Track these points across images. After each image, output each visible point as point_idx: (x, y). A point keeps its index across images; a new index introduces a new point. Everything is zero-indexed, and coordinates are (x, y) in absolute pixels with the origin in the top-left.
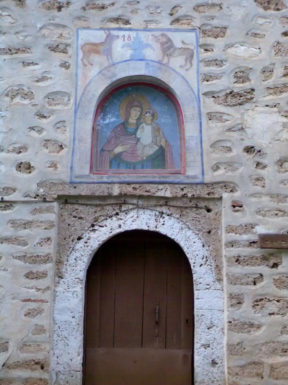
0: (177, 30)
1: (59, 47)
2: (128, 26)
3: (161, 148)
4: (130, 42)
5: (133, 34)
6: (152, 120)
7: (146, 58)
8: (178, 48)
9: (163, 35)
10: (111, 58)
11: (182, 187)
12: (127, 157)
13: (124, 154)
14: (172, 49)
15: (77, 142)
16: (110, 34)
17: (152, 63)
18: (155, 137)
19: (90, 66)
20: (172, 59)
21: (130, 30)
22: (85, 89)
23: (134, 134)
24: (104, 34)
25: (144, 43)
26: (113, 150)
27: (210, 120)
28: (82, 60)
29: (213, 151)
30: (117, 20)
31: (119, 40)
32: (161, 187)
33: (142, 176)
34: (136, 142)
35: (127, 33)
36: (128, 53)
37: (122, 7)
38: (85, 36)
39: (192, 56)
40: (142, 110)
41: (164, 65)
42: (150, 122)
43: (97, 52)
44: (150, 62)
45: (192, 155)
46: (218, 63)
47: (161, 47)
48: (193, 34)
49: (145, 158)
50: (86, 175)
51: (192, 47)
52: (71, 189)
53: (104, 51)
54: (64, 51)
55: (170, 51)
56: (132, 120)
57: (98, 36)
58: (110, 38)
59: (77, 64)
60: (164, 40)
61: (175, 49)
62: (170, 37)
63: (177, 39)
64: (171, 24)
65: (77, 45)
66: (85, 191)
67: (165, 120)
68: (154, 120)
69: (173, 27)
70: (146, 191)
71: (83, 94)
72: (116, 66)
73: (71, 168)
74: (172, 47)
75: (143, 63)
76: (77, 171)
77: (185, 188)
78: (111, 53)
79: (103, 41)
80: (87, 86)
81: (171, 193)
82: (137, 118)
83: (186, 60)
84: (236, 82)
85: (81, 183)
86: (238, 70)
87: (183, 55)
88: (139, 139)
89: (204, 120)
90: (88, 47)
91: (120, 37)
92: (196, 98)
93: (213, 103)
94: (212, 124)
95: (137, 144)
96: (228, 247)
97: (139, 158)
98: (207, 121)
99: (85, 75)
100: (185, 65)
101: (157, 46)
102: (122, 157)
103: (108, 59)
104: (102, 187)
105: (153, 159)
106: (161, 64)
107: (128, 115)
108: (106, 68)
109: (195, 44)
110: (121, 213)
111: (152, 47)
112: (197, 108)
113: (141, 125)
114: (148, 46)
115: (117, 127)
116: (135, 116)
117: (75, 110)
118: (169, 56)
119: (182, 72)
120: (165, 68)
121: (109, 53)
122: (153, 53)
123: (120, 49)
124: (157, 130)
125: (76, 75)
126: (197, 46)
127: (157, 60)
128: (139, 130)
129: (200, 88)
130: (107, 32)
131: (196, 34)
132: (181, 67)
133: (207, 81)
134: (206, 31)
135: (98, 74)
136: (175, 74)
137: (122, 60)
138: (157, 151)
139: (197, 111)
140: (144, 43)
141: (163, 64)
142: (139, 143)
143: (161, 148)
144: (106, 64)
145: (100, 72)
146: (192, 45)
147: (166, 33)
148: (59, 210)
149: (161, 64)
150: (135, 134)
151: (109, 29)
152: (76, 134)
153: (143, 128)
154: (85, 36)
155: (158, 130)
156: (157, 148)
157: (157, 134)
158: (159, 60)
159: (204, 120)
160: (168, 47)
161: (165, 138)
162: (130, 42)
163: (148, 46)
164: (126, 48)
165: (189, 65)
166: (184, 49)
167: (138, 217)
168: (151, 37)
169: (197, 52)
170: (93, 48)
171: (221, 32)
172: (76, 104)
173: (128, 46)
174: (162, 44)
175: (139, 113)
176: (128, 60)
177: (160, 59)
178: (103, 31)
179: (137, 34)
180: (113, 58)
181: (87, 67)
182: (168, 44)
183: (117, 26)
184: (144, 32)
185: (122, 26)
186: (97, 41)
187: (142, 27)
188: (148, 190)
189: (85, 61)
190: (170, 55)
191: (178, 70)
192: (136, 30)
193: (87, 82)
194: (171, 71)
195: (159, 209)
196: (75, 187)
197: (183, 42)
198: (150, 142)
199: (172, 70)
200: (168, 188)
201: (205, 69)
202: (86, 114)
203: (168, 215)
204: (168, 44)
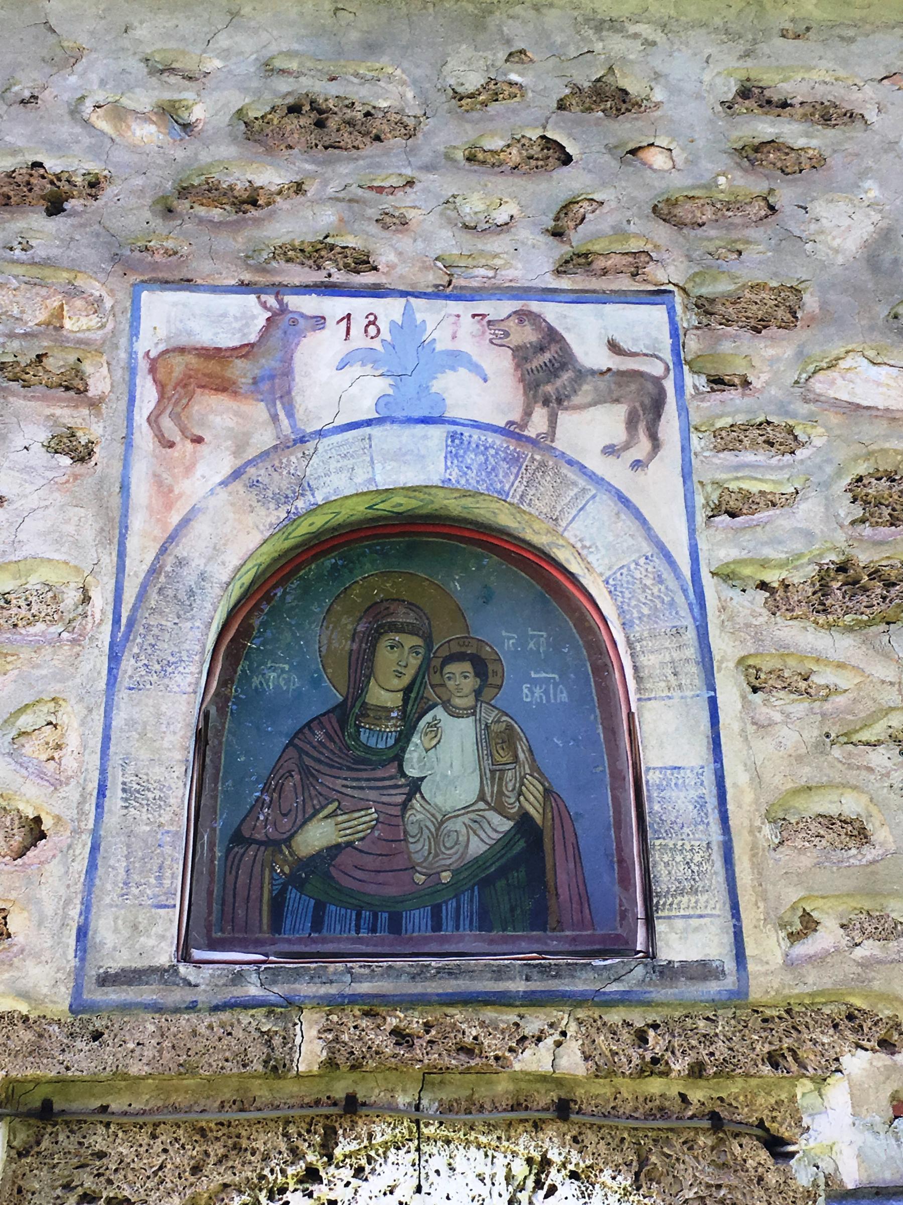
0: (580, 297)
1: (48, 362)
2: (368, 278)
3: (524, 822)
4: (376, 344)
5: (389, 310)
6: (478, 693)
7: (449, 414)
8: (593, 372)
9: (522, 316)
10: (290, 415)
11: (639, 1024)
12: (359, 874)
13: (343, 858)
14: (566, 376)
15: (115, 800)
16: (284, 309)
17: (476, 435)
18: (493, 772)
19: (189, 446)
20: (565, 418)
21: (376, 292)
22: (163, 550)
23: (392, 760)
24: (258, 310)
25: (439, 347)
26: (288, 841)
27: (755, 690)
28: (153, 420)
29: (781, 843)
30: (316, 253)
31: (325, 333)
32: (534, 1023)
33: (439, 970)
34: (400, 799)
35: (360, 306)
36: (366, 392)
37: (337, 199)
38: (170, 317)
39: (657, 406)
40: (429, 645)
41: (533, 442)
42: (470, 701)
43: (224, 387)
44: (467, 431)
45: (679, 858)
46: (779, 439)
47: (518, 366)
48: (657, 314)
49: (446, 877)
50: (153, 970)
51: (656, 369)
52: (79, 1044)
53: (255, 381)
54: (73, 385)
55: (559, 383)
56: (384, 694)
57: (224, 318)
58: (282, 327)
59: (128, 441)
60: (528, 335)
61: (582, 374)
62: (553, 324)
63: (588, 333)
64: (558, 272)
65: (132, 354)
66: (149, 1053)
67: (538, 692)
68: (488, 692)
69: (564, 283)
70: (462, 1049)
71: (154, 571)
72: (311, 445)
73: (82, 933)
74: (563, 366)
75: (437, 433)
76: (115, 949)
77: (655, 1026)
78: (289, 392)
79: (253, 338)
80: (173, 538)
81: (586, 1059)
82: (406, 680)
83: (631, 423)
84: (863, 521)
85: (125, 1008)
86: (862, 469)
87: (617, 401)
88: (415, 786)
89: (730, 691)
90: (179, 365)
91: (331, 323)
92: (685, 591)
93: (765, 612)
94: (775, 706)
95: (405, 806)
96: (620, 386)
97: (420, 878)
98: (744, 697)
99: (165, 492)
100: (627, 446)
101: (498, 364)
102: (334, 872)
103: (275, 418)
104: (238, 1033)
105: (486, 883)
106: (519, 438)
107: (361, 667)
108: (265, 455)
109: (668, 356)
110: (332, 1169)
111: (476, 368)
112: (691, 635)
113: (428, 718)
114: (456, 359)
115: (308, 725)
116: (399, 675)
117: (112, 645)
118: (557, 403)
119: (614, 472)
120: (538, 457)
121: (277, 387)
122: (484, 391)
123: (332, 374)
124: (499, 743)
125: (125, 488)
126: (678, 364)
127: (502, 424)
128: (416, 739)
129: (703, 545)
130: (271, 301)
131: (671, 312)
132: (610, 450)
133: (733, 515)
134: (712, 301)
135: (224, 483)
136: (582, 482)
137: (341, 421)
138: (507, 840)
139: (692, 652)
140: (439, 347)
141: (528, 439)
142: (416, 803)
143: (524, 822)
144: (265, 439)
145: (236, 474)
146: (657, 357)
147: (535, 306)
148: (10, 1160)
149: (519, 438)
150: (399, 759)
151: (279, 290)
152: (115, 759)
153: (434, 726)
154: (170, 317)
155: (508, 739)
156: (506, 825)
157: (504, 757)
158: (511, 423)
159: (730, 691)
160: (547, 370)
161: (542, 778)
162: (376, 344)
163: (456, 359)
164: (355, 370)
165: (644, 444)
166: (621, 374)
167: (419, 1189)
168: (468, 325)
169: (680, 389)
170: (205, 371)
171: (777, 312)
172: (116, 621)
173: (367, 357)
174: (521, 355)
175: (415, 662)
176: (369, 423)
177: (516, 416)
178: (253, 298)
179: (408, 312)
180: (300, 414)
181: (175, 453)
182: (547, 356)
183: (319, 277)
184: (440, 303)
185: (339, 277)
186: (227, 341)
187: (430, 279)
188: (469, 1040)
189: (167, 423)
190: (559, 401)
191: (596, 463)
192: (404, 294)
193: (175, 519)
194: (565, 470)
195: (525, 1145)
196: (97, 1036)
197: (614, 347)
198: (473, 797)
199: (571, 462)
200: (572, 1029)
201: (716, 467)
202: (166, 668)
203: (574, 1175)
204: (547, 356)
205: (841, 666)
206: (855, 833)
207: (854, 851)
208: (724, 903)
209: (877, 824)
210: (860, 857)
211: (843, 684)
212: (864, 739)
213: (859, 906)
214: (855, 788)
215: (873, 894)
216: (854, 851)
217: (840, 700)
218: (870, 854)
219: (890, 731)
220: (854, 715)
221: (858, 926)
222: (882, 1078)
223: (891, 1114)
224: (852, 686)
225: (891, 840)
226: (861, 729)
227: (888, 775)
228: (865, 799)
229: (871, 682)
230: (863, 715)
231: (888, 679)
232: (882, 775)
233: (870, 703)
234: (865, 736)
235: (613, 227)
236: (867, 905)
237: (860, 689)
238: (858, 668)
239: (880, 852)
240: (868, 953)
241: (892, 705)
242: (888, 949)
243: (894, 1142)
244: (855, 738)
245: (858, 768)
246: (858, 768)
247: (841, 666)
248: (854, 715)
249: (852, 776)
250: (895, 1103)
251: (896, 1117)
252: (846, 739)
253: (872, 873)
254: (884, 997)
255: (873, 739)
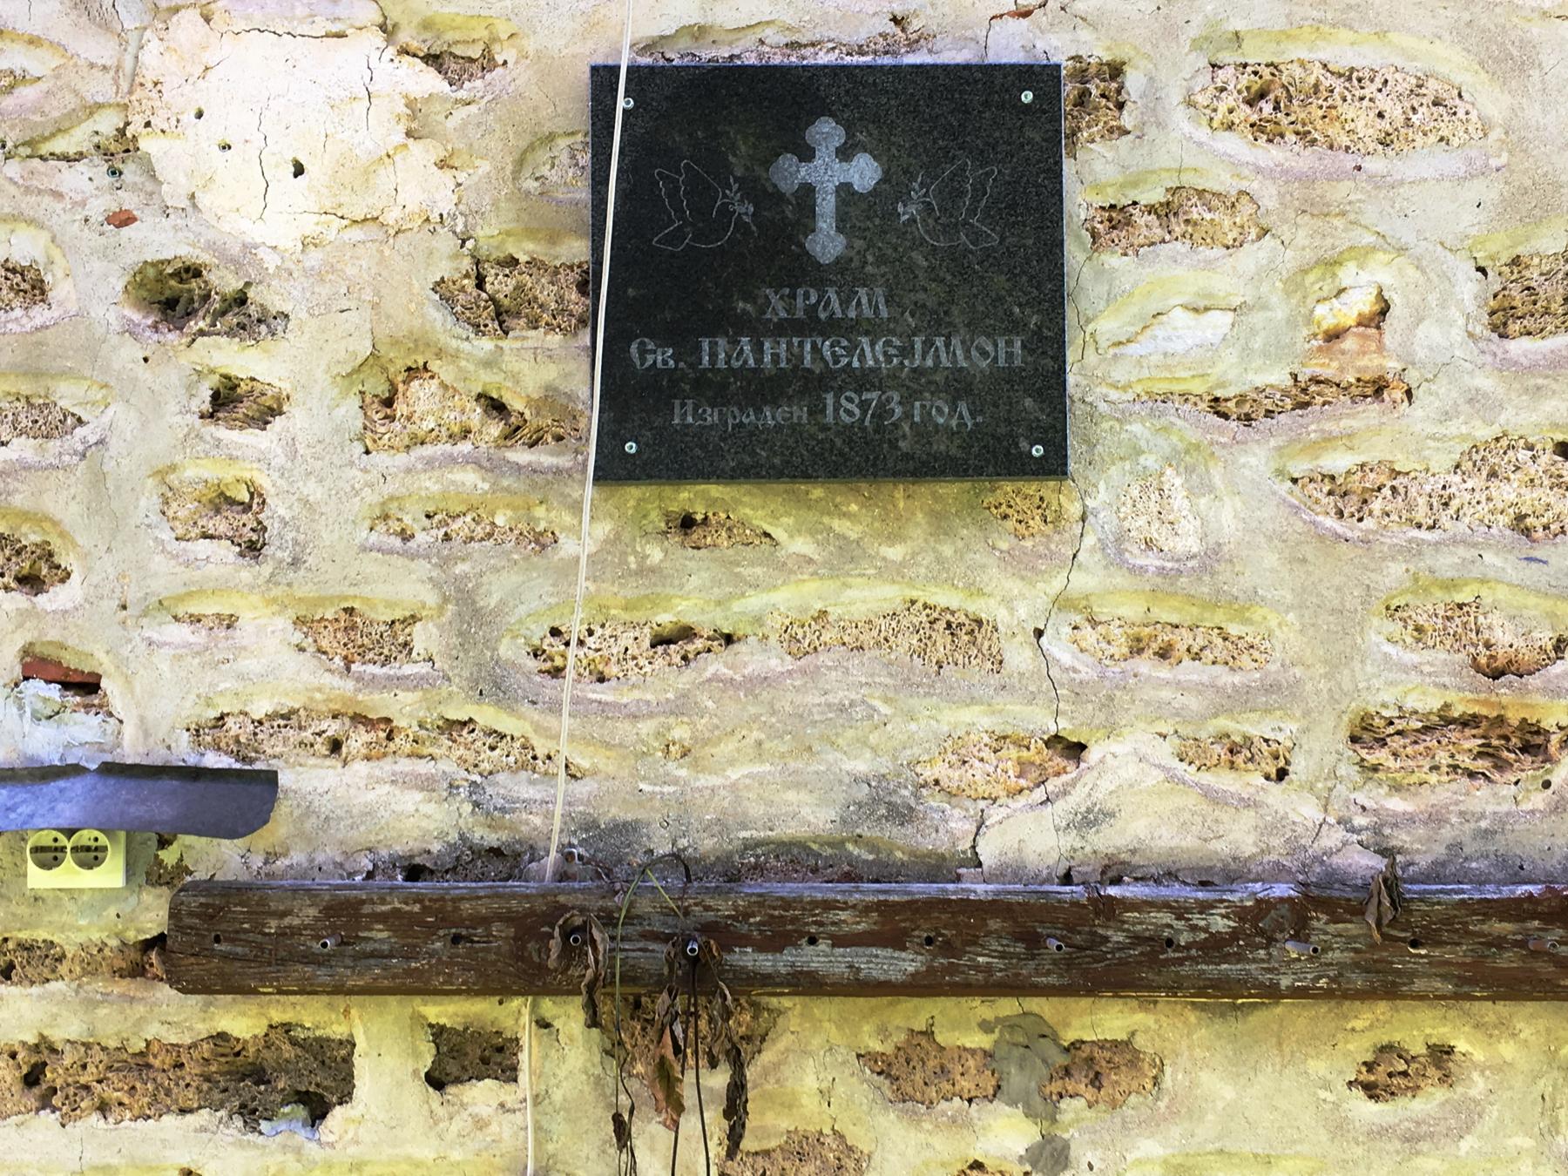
205: (34, 41)
206: (24, 286)
207: (18, 312)
208: (750, 493)
209: (60, 274)
210: (25, 320)
211: (35, 70)
212: (58, 151)
213: (14, 390)
214: (31, 222)
215: (37, 374)
216: (18, 312)
217: (27, 93)
218: (40, 315)
219: (96, 139)
220: (43, 113)
221: (10, 417)
222: (11, 627)
223: (18, 672)
224: (48, 72)
225: (73, 297)
226: (53, 135)
227: (83, 204)
228: (44, 237)
229: (75, 65)
230: (56, 114)
231: (100, 62)
232: (75, 204)
233: (69, 97)
234: (60, 145)
235: (1288, 294)
236: (25, 389)
237: (58, 77)
238: (59, 44)
239: (56, 315)
240: (15, 457)
241: (100, 99)
242: (44, 450)
243: (15, 710)
244: (45, 149)
245: (40, 192)
246: (40, 192)
247: (34, 41)
248: (43, 113)
249: (28, 204)
250: (28, 659)
251: (26, 678)
252: (28, 151)
253: (39, 344)
254: (26, 516)
255: (72, 151)
